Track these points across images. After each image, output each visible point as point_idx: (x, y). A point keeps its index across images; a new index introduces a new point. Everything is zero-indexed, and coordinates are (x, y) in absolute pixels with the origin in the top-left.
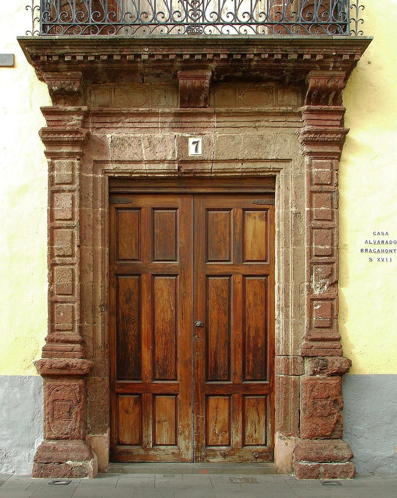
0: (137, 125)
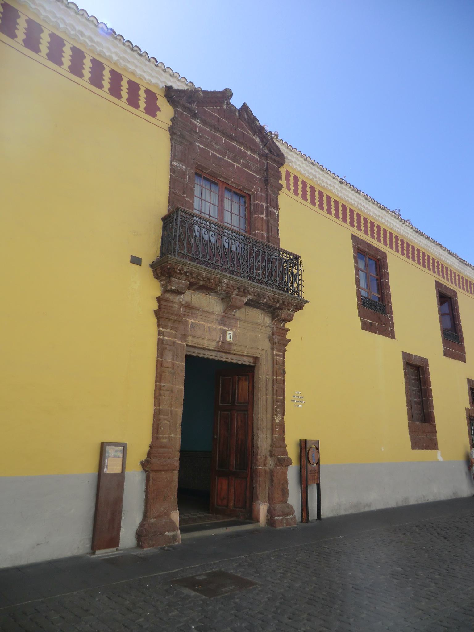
0: (204, 318)
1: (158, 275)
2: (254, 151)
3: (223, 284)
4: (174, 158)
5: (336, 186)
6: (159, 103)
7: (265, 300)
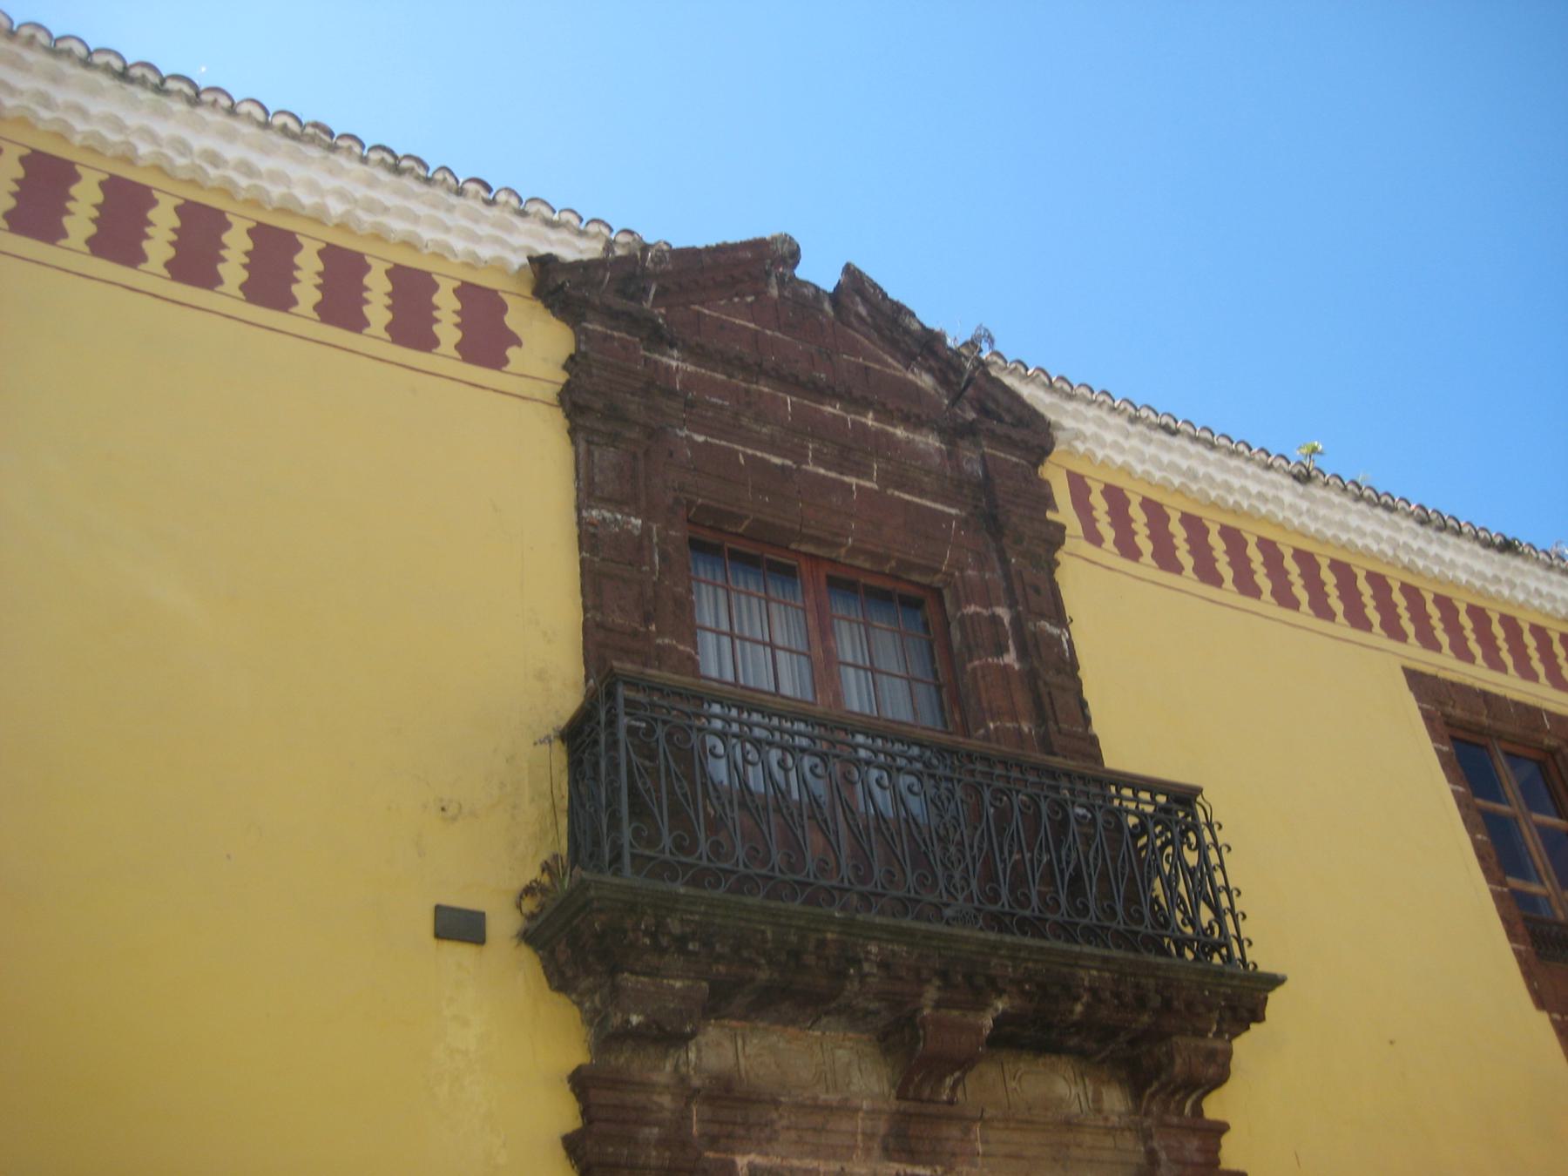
1: (562, 974)
2: (914, 422)
3: (866, 967)
4: (590, 495)
5: (1287, 497)
6: (512, 320)
7: (1079, 1008)
